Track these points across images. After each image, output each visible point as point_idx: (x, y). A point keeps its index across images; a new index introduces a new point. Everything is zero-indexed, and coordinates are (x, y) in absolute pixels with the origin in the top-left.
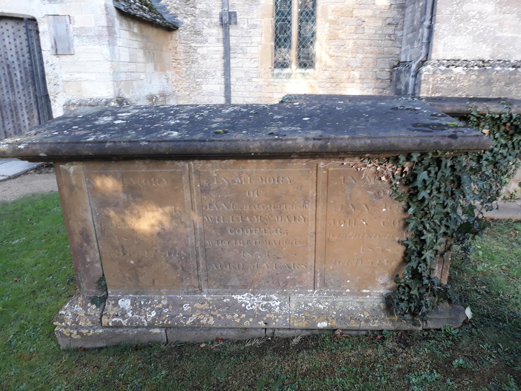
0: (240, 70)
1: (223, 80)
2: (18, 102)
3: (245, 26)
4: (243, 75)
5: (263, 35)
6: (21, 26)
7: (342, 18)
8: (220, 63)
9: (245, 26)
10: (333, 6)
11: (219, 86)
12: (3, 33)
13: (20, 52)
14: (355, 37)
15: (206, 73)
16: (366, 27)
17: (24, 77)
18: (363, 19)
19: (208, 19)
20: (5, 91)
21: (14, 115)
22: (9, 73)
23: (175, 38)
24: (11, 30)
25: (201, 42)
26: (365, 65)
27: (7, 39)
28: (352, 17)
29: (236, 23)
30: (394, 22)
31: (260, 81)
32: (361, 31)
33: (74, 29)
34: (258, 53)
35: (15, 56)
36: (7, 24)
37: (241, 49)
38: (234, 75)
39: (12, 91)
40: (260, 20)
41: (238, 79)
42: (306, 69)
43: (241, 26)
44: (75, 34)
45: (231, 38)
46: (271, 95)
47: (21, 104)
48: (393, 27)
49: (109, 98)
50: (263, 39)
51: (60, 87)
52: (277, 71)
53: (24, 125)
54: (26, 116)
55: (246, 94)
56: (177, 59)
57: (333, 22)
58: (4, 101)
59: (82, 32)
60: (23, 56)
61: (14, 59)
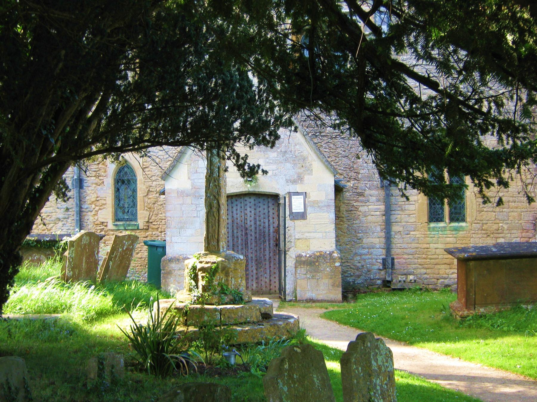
8: (381, 219)
13: (257, 218)
22: (246, 234)
23: (339, 199)
27: (249, 209)
34: (415, 210)
41: (396, 233)
46: (428, 245)
47: (252, 257)
51: (292, 243)
56: (340, 217)
60: (260, 221)
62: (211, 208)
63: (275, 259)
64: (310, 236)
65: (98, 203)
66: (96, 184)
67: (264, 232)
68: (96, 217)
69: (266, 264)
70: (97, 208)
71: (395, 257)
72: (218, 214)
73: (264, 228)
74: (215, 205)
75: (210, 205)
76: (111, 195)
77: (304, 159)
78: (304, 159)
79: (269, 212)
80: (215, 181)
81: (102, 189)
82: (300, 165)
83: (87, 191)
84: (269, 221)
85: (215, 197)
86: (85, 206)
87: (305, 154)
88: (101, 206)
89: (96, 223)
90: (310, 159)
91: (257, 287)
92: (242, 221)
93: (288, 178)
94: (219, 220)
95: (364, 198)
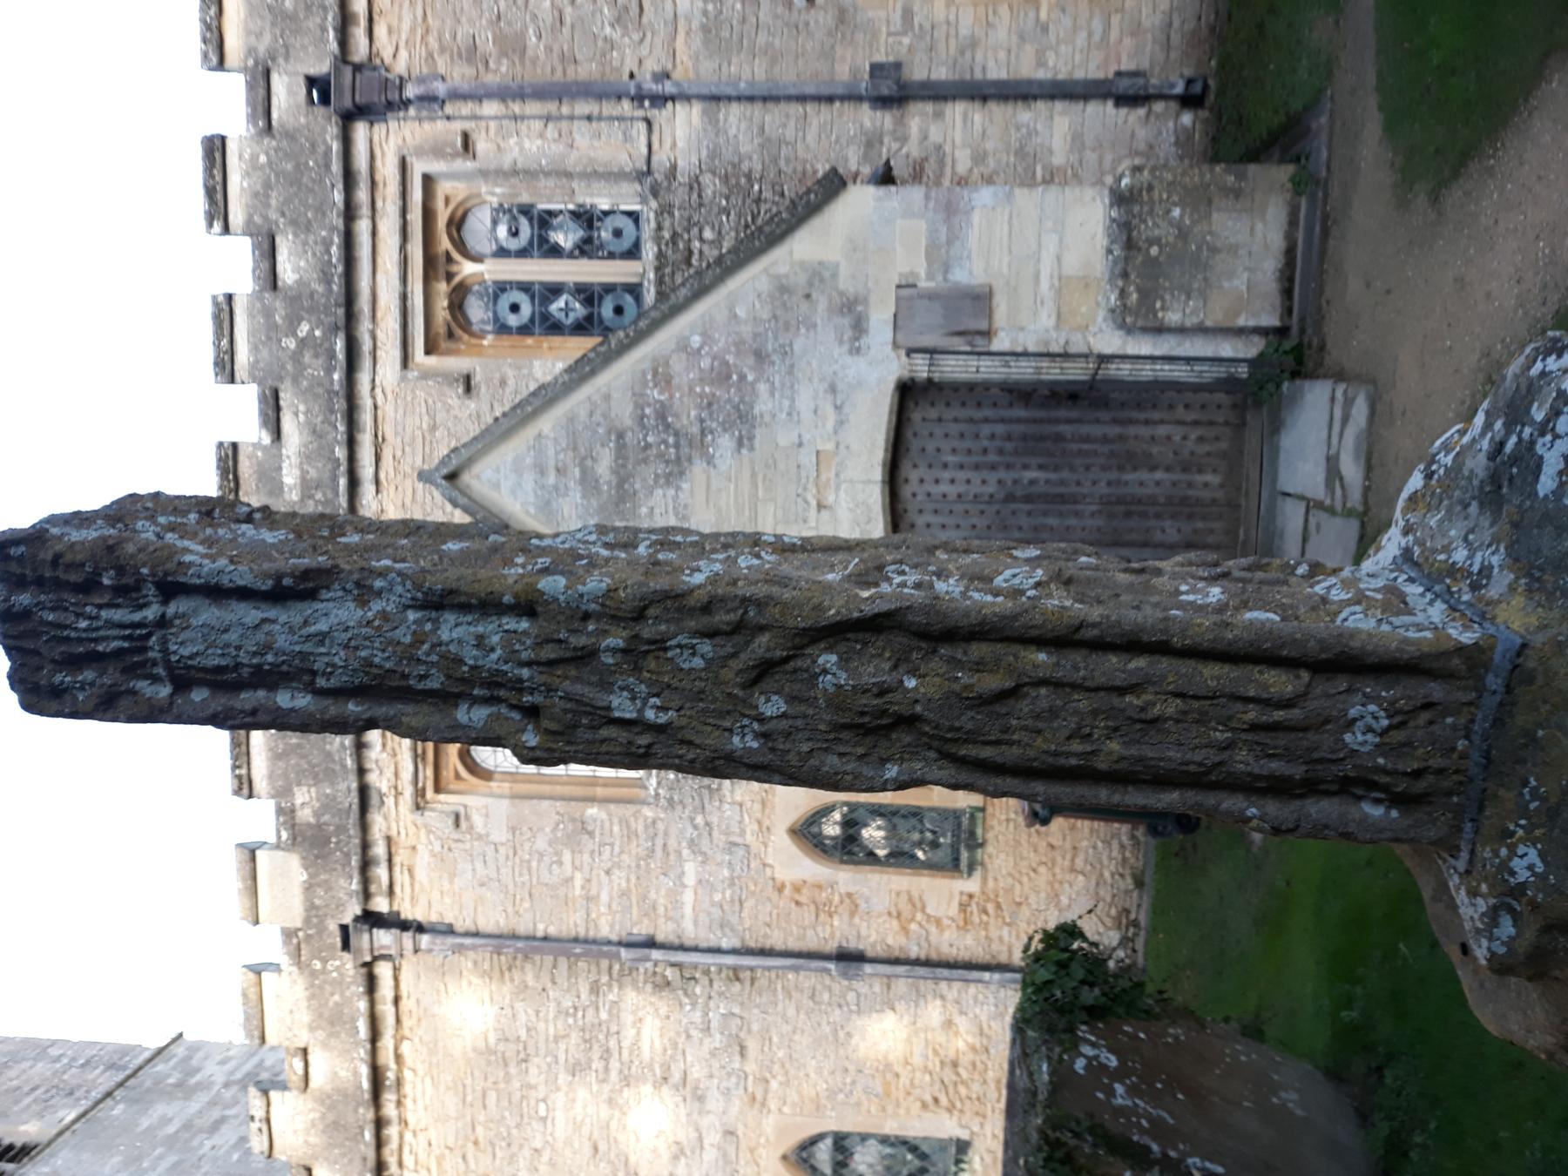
0: (1017, 57)
1: (1041, 105)
2: (1102, 489)
3: (906, 40)
4: (1029, 49)
6: (916, 416)
9: (906, 40)
11: (1057, 119)
12: (929, 495)
13: (975, 459)
15: (1020, 153)
17: (1040, 460)
19: (886, 140)
20: (1072, 521)
21: (1142, 508)
22: (1028, 499)
24: (922, 471)
25: (941, 163)
27: (943, 488)
29: (898, 66)
33: (930, 276)
35: (985, 474)
36: (906, 481)
37: (962, 53)
38: (1027, 69)
39: (1075, 502)
41: (1041, 63)
43: (904, 51)
44: (940, 278)
45: (934, 76)
47: (1109, 484)
49: (1107, 201)
54: (1143, 475)
55: (1081, 39)
58: (1099, 530)
59: (940, 254)
60: (985, 451)
61: (992, 477)
62: (909, 721)
63: (1123, 404)
64: (1052, 277)
65: (906, 914)
66: (852, 914)
67: (1024, 438)
68: (946, 922)
69: (1136, 437)
70: (919, 916)
71: (1113, 69)
72: (979, 650)
73: (1009, 438)
74: (873, 670)
75: (866, 731)
76: (885, 877)
77: (783, 288)
78: (783, 288)
79: (956, 420)
80: (586, 656)
81: (867, 901)
82: (804, 306)
83: (872, 939)
84: (986, 420)
85: (763, 671)
86: (914, 952)
87: (764, 285)
88: (914, 905)
89: (961, 923)
90: (783, 269)
91: (1215, 471)
92: (982, 512)
93: (846, 347)
94: (1064, 639)
95: (932, 160)
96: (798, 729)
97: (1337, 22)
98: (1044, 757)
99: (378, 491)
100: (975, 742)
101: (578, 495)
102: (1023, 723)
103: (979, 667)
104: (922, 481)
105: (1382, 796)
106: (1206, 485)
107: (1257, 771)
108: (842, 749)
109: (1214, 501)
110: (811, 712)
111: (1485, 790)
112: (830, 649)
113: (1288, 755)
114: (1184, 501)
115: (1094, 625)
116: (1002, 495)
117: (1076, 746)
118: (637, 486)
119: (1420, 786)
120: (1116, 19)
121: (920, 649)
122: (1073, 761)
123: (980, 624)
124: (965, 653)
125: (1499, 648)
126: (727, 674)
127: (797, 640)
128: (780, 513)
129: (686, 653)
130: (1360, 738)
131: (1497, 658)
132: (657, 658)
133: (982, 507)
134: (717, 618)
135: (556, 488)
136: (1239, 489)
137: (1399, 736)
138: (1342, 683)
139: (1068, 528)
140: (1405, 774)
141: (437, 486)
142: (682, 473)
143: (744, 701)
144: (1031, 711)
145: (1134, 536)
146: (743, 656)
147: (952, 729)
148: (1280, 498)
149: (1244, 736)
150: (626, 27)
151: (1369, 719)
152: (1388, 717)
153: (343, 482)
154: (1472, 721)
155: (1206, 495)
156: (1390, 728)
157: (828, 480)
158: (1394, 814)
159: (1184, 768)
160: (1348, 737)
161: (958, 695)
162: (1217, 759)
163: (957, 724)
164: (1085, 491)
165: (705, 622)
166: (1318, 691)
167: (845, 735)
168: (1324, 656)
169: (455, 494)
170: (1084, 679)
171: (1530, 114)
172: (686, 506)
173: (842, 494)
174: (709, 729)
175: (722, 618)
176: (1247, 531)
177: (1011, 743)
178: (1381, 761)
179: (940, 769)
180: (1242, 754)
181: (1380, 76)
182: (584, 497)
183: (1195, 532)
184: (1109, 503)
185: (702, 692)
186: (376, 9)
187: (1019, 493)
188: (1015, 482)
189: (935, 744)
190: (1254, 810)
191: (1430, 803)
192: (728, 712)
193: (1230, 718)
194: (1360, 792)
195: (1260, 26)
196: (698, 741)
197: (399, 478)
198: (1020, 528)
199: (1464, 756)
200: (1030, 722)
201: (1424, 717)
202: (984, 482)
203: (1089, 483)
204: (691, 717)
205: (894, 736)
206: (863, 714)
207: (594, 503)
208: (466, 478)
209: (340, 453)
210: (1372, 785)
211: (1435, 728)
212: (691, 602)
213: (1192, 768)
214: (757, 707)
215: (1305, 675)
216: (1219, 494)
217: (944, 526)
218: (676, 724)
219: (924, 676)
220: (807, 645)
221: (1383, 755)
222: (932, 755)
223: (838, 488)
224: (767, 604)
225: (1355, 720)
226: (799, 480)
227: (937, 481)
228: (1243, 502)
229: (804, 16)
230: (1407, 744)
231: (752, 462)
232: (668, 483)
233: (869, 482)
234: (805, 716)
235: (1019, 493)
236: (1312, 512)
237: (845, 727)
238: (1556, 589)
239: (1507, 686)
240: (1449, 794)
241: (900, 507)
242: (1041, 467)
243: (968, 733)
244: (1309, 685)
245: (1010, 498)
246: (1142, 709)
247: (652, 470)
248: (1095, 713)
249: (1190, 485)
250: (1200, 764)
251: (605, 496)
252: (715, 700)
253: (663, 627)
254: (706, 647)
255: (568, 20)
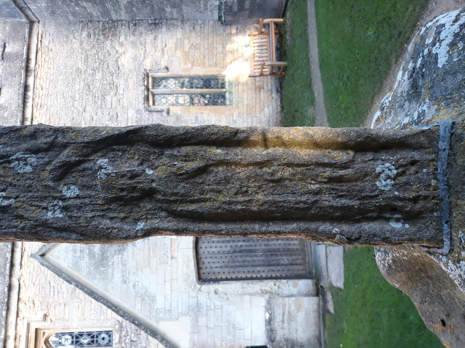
2: (263, 247)
5: (202, 112)
7: (190, 58)
10: (182, 65)
12: (208, 252)
14: (202, 49)
16: (196, 43)
18: (190, 45)
20: (255, 258)
22: (240, 252)
24: (206, 244)
26: (221, 42)
27: (213, 249)
28: (189, 52)
30: (192, 26)
31: (235, 114)
32: (198, 46)
35: (226, 244)
36: (201, 248)
39: (255, 252)
40: (192, 115)
42: (226, 82)
48: (196, 26)
50: (205, 112)
52: (228, 102)
53: (283, 244)
57: (193, 64)
58: (263, 261)
61: (229, 245)
72: (184, 150)
92: (226, 257)
96: (86, 205)
97: (314, 108)
98: (224, 206)
99: (21, 268)
100: (187, 202)
101: (88, 259)
102: (211, 187)
103: (187, 158)
104: (206, 248)
105: (400, 216)
106: (294, 244)
107: (335, 204)
108: (112, 215)
109: (297, 249)
110: (93, 193)
111: (451, 203)
112: (103, 156)
113: (348, 195)
114: (288, 250)
115: (243, 132)
116: (232, 251)
117: (240, 198)
118: (108, 255)
119: (418, 206)
120: (254, 119)
121: (154, 153)
122: (239, 207)
123: (184, 134)
124: (179, 152)
125: (442, 128)
126: (46, 174)
127: (85, 150)
128: (158, 261)
129: (22, 163)
130: (384, 183)
131: (442, 133)
132: (4, 168)
133: (226, 255)
134: (39, 141)
135: (80, 257)
136: (304, 245)
137: (403, 179)
138: (370, 156)
139: (254, 261)
140: (409, 200)
141: (37, 259)
142: (124, 249)
143: (54, 189)
144: (215, 180)
145: (274, 262)
146: (54, 162)
147: (173, 194)
148: (317, 246)
149: (325, 186)
150: (112, 121)
151: (387, 172)
152: (397, 169)
153: (8, 265)
154: (436, 169)
155: (294, 247)
156: (398, 175)
157: (175, 248)
158: (407, 226)
159: (298, 206)
160: (378, 183)
161: (175, 173)
162: (314, 199)
163: (175, 191)
164: (258, 248)
165: (31, 144)
166: (359, 160)
167: (113, 206)
168: (359, 140)
169: (43, 261)
170: (241, 159)
171: (372, 114)
172: (125, 261)
173: (179, 253)
174: (34, 208)
175: (41, 141)
176: (309, 258)
177: (205, 200)
178: (396, 193)
179: (169, 222)
180: (326, 197)
181: (328, 118)
182: (89, 260)
183: (293, 260)
184: (266, 252)
185: (30, 186)
186: (34, 117)
187: (237, 250)
188: (236, 246)
189: (165, 206)
190: (336, 229)
191: (423, 218)
192: (46, 197)
193: (317, 176)
194: (388, 215)
195: (293, 116)
196: (26, 216)
197: (29, 263)
198: (239, 262)
199: (436, 188)
200: (214, 187)
201: (413, 169)
202: (226, 247)
203: (258, 246)
204: (23, 202)
205: (142, 205)
206: (122, 190)
207: (93, 261)
208: (48, 255)
209: (9, 255)
210: (394, 210)
211: (419, 175)
212: (25, 132)
213: (301, 205)
214: (61, 192)
215: (351, 153)
216: (299, 247)
217: (214, 262)
218: (14, 205)
219: (156, 168)
220: (91, 154)
221: (397, 190)
222: (164, 214)
223: (178, 251)
224: (68, 132)
225: (380, 173)
226: (165, 248)
227: (211, 247)
228: (306, 249)
229: (166, 118)
230: (406, 184)
231: (149, 244)
232: (119, 253)
233: (188, 248)
234: (90, 197)
235: (237, 250)
236: (327, 247)
237: (113, 200)
238: (461, 98)
239: (450, 145)
240: (432, 211)
241: (199, 257)
242: (243, 241)
243: (182, 195)
244: (354, 157)
245: (235, 252)
246: (272, 174)
247: (114, 249)
248: (248, 178)
249: (289, 245)
250: (305, 203)
251: (97, 259)
252: (38, 191)
253: (8, 149)
254: (33, 159)
255: (95, 119)
